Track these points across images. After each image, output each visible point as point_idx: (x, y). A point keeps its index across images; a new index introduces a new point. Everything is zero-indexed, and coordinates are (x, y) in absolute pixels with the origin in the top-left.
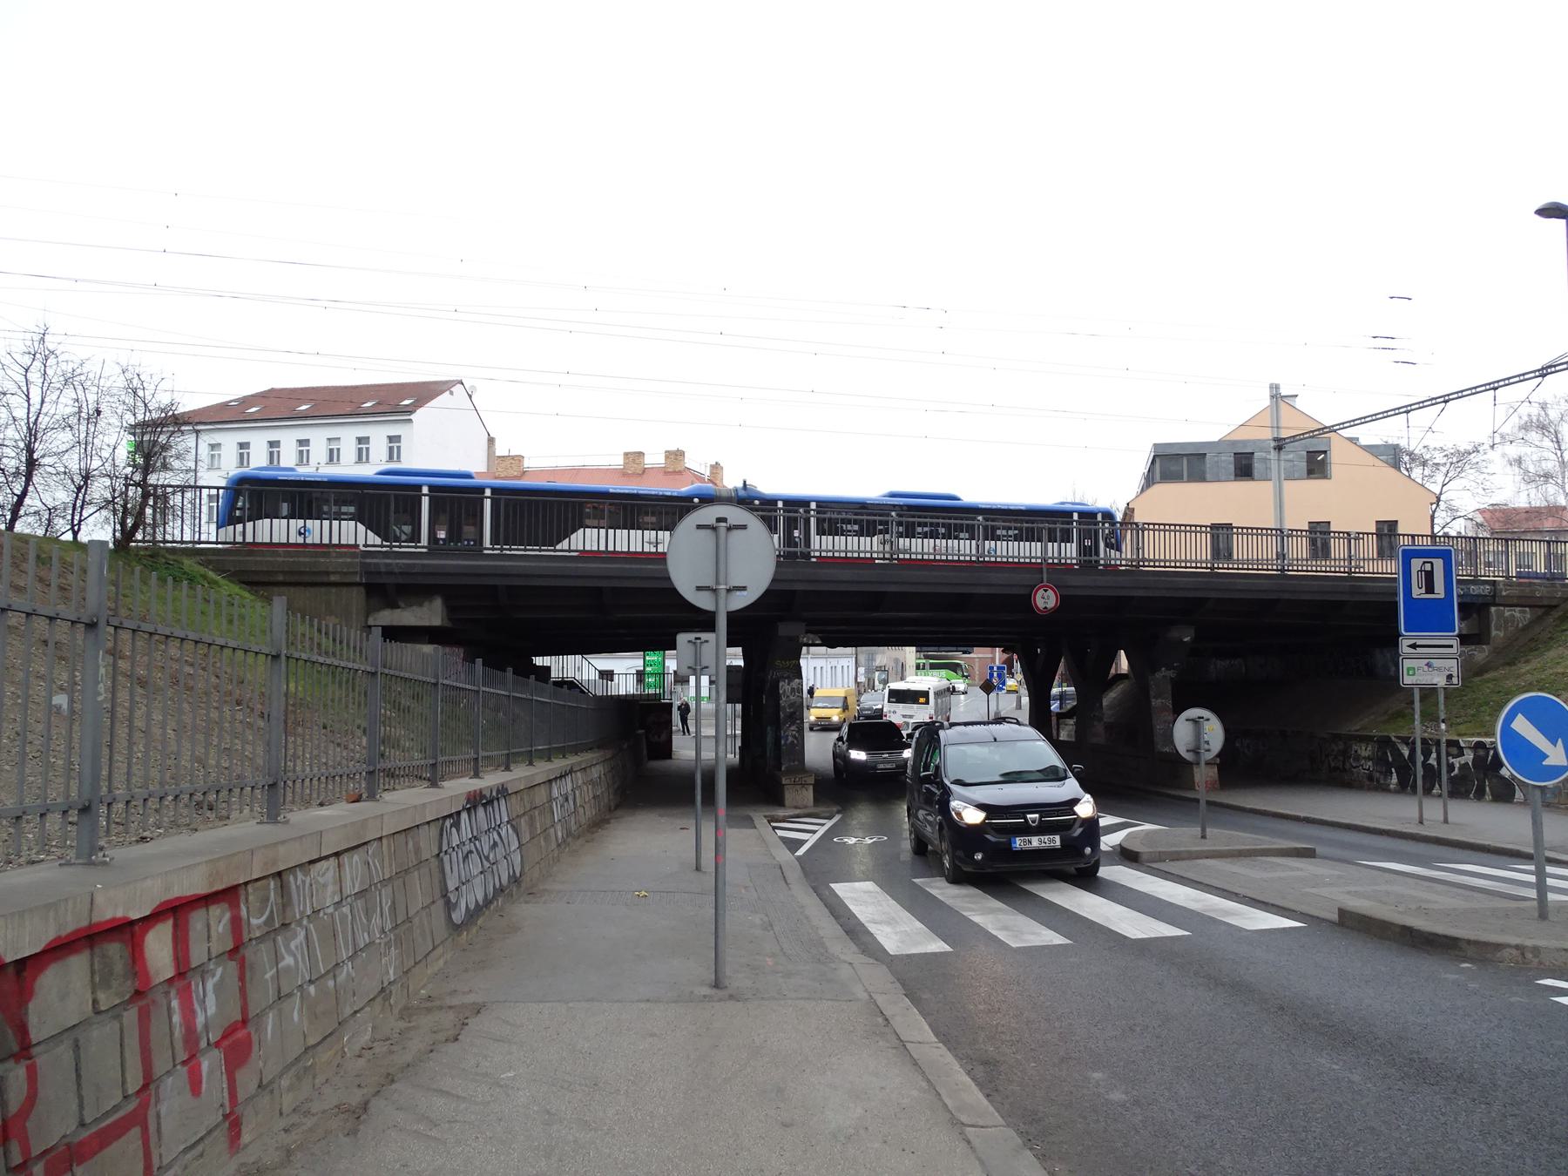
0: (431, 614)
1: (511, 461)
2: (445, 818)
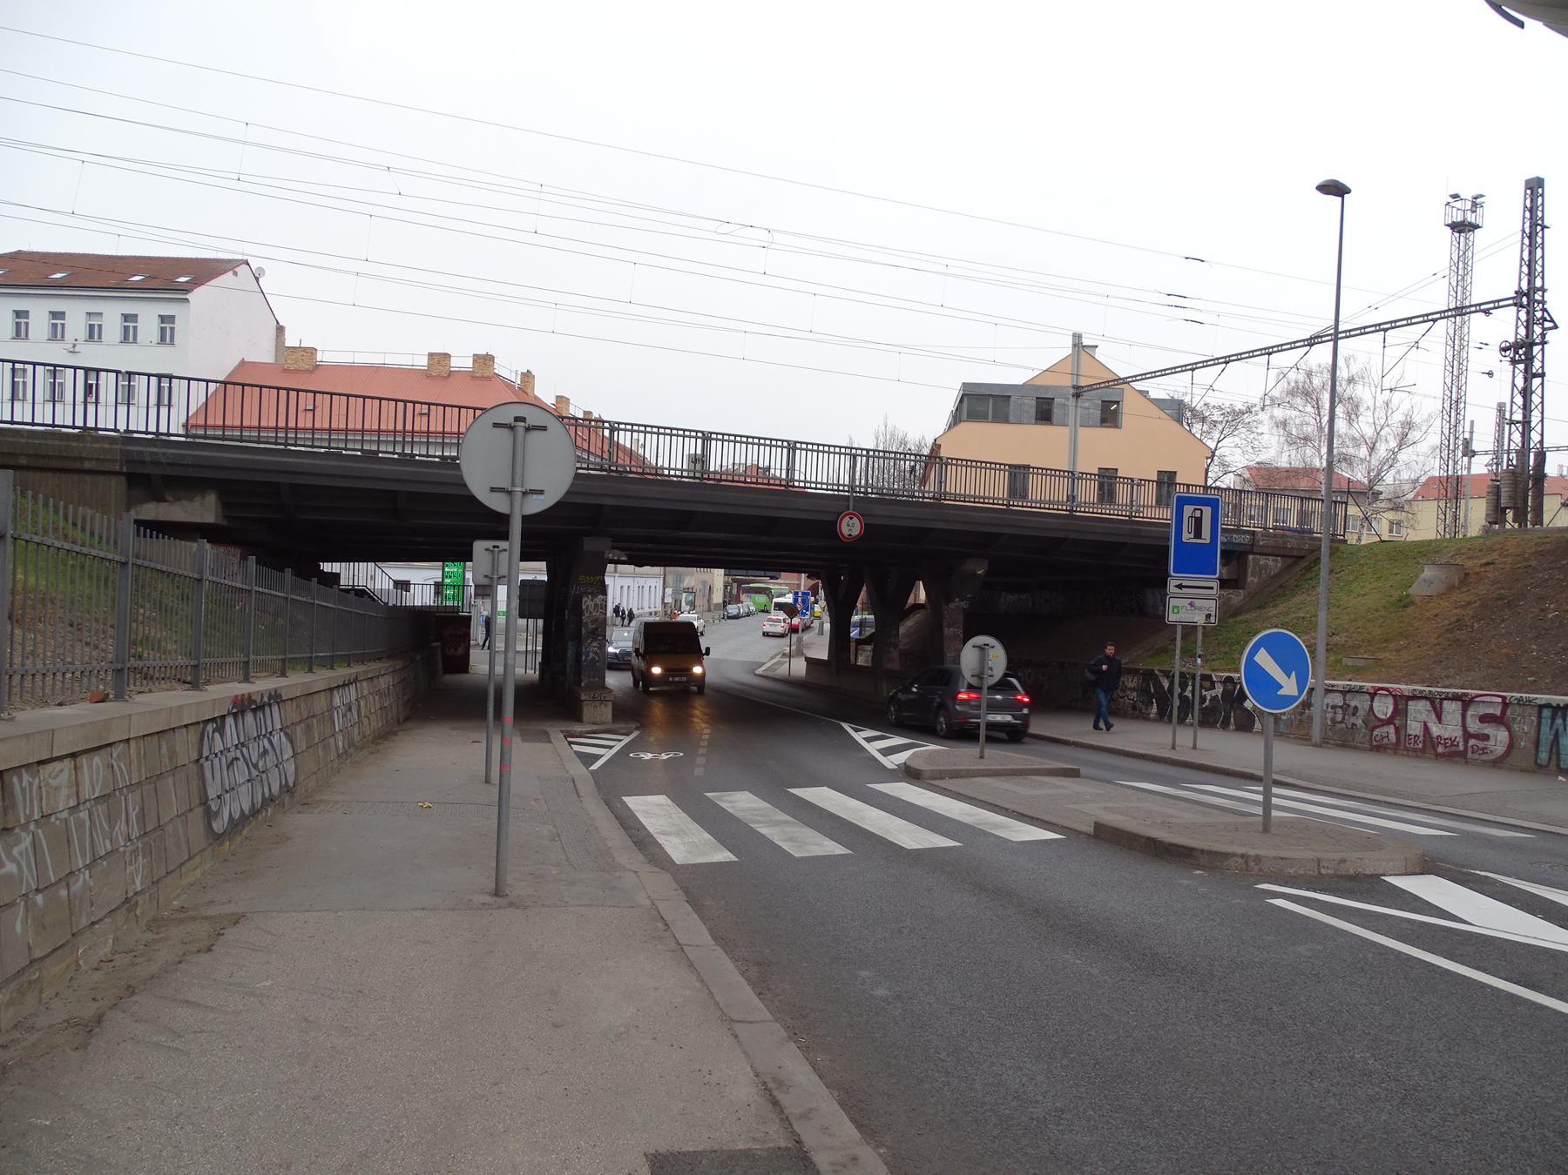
0: (204, 509)
1: (302, 353)
2: (207, 722)
